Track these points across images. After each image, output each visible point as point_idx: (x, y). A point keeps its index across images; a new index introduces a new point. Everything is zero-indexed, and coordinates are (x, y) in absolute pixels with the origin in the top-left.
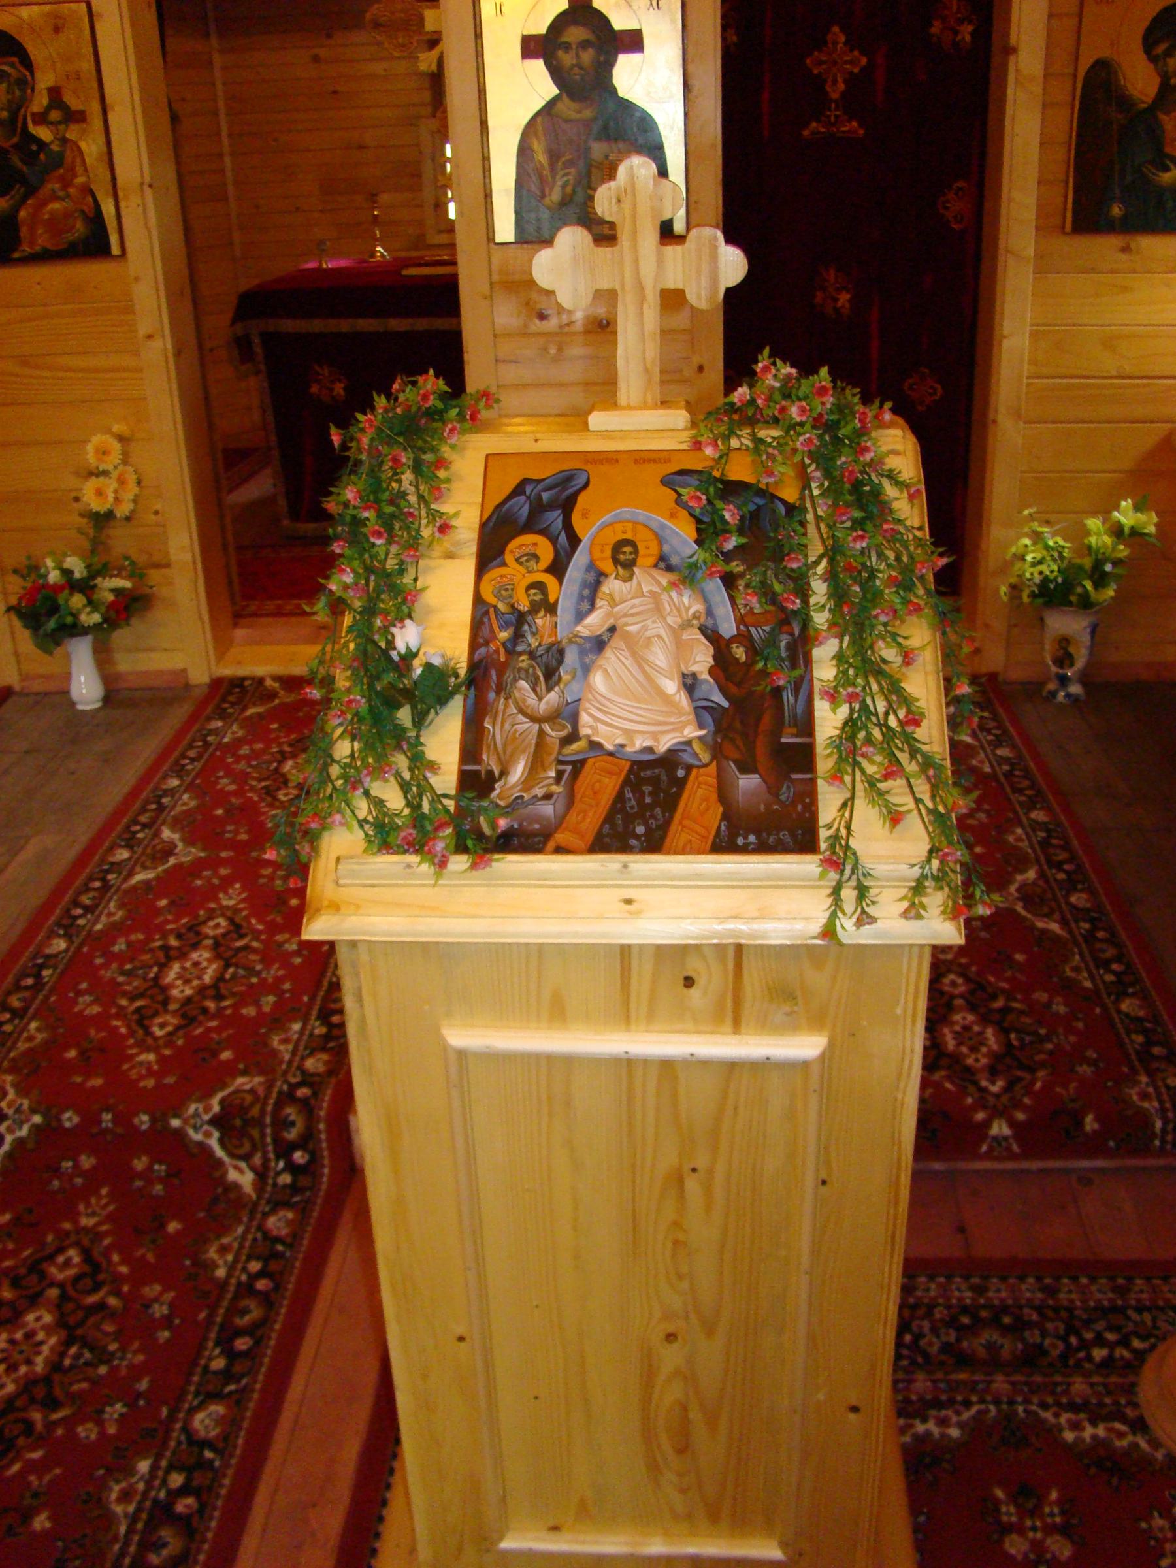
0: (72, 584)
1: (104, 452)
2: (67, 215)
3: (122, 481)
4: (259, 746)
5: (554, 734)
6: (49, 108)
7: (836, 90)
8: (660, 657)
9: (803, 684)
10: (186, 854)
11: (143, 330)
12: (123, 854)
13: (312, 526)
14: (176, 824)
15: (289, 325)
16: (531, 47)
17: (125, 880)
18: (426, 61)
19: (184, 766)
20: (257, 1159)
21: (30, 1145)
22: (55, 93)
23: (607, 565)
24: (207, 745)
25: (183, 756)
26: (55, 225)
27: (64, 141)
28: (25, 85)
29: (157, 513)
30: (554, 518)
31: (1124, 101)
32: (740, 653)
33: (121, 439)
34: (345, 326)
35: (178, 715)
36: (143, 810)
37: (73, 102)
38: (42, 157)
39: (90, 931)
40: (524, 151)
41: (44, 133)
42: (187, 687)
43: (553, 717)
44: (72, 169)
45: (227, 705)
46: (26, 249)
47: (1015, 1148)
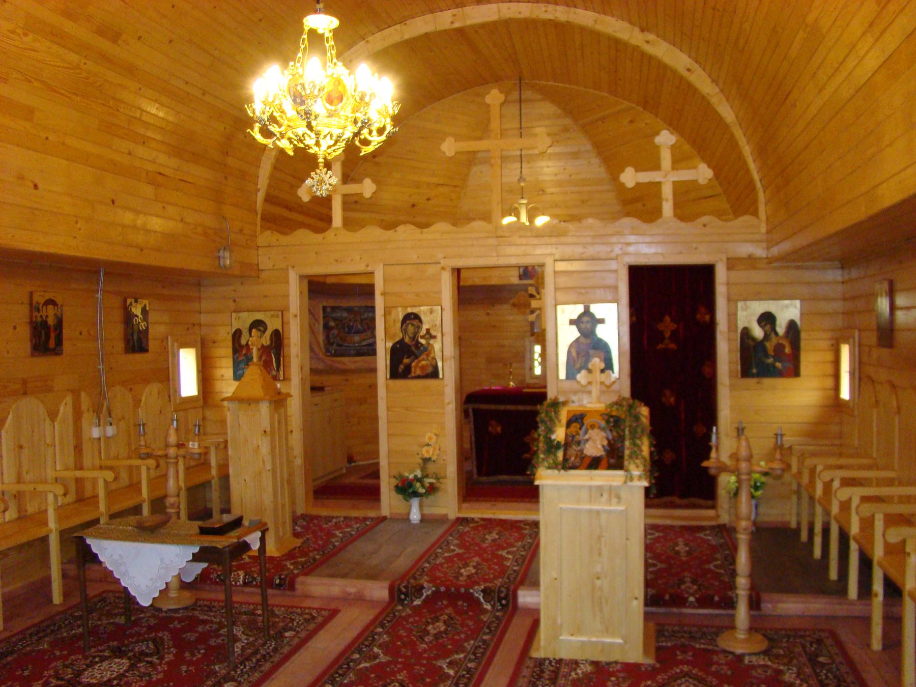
0: (417, 479)
1: (430, 439)
2: (427, 365)
3: (434, 449)
4: (417, 618)
5: (579, 453)
6: (426, 334)
7: (667, 334)
8: (598, 442)
9: (623, 446)
10: (383, 658)
11: (447, 401)
12: (357, 656)
13: (485, 478)
14: (380, 646)
15: (484, 407)
16: (572, 322)
17: (357, 666)
18: (532, 318)
19: (362, 648)
20: (492, 603)
21: (430, 597)
22: (428, 331)
23: (589, 428)
24: (395, 615)
25: (384, 619)
26: (423, 368)
27: (429, 344)
28: (419, 328)
29: (444, 460)
30: (580, 421)
31: (754, 339)
32: (612, 442)
33: (436, 435)
34: (502, 407)
35: (440, 531)
36: (366, 640)
37: (433, 333)
38: (422, 348)
39: (341, 683)
40: (569, 352)
41: (423, 341)
42: (448, 520)
43: (579, 451)
44: (430, 352)
45: (386, 622)
46: (413, 374)
47: (696, 605)
